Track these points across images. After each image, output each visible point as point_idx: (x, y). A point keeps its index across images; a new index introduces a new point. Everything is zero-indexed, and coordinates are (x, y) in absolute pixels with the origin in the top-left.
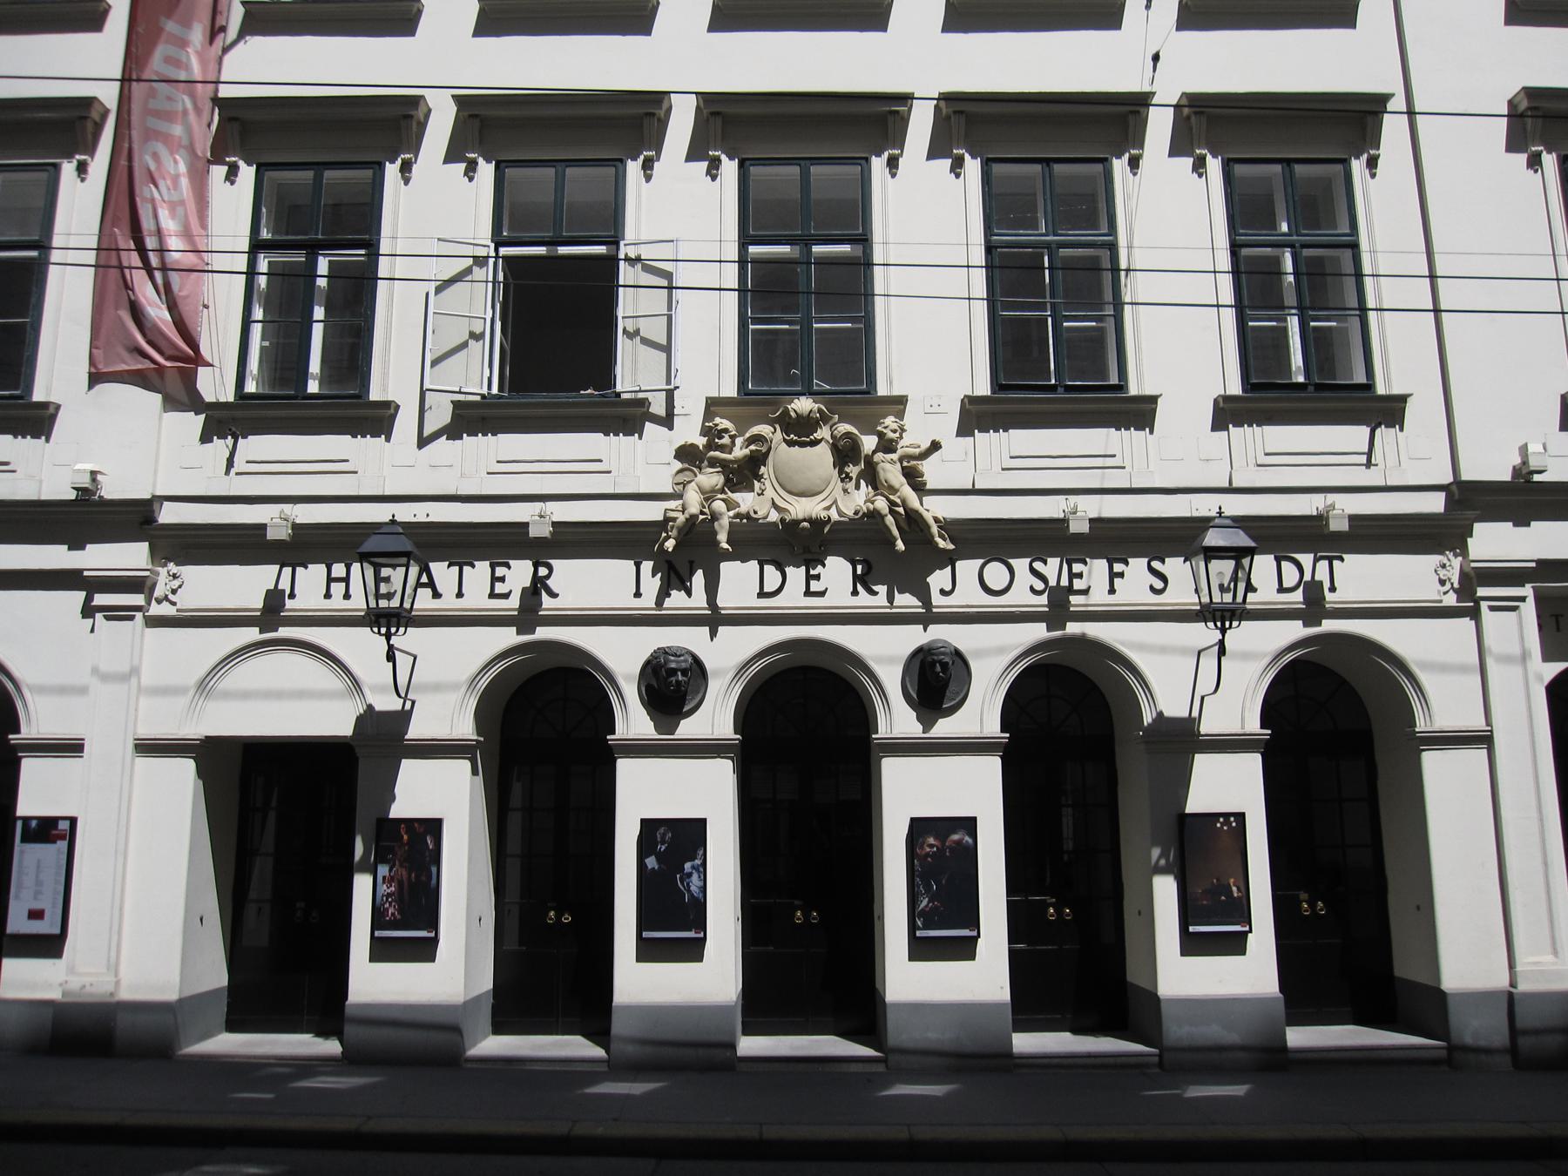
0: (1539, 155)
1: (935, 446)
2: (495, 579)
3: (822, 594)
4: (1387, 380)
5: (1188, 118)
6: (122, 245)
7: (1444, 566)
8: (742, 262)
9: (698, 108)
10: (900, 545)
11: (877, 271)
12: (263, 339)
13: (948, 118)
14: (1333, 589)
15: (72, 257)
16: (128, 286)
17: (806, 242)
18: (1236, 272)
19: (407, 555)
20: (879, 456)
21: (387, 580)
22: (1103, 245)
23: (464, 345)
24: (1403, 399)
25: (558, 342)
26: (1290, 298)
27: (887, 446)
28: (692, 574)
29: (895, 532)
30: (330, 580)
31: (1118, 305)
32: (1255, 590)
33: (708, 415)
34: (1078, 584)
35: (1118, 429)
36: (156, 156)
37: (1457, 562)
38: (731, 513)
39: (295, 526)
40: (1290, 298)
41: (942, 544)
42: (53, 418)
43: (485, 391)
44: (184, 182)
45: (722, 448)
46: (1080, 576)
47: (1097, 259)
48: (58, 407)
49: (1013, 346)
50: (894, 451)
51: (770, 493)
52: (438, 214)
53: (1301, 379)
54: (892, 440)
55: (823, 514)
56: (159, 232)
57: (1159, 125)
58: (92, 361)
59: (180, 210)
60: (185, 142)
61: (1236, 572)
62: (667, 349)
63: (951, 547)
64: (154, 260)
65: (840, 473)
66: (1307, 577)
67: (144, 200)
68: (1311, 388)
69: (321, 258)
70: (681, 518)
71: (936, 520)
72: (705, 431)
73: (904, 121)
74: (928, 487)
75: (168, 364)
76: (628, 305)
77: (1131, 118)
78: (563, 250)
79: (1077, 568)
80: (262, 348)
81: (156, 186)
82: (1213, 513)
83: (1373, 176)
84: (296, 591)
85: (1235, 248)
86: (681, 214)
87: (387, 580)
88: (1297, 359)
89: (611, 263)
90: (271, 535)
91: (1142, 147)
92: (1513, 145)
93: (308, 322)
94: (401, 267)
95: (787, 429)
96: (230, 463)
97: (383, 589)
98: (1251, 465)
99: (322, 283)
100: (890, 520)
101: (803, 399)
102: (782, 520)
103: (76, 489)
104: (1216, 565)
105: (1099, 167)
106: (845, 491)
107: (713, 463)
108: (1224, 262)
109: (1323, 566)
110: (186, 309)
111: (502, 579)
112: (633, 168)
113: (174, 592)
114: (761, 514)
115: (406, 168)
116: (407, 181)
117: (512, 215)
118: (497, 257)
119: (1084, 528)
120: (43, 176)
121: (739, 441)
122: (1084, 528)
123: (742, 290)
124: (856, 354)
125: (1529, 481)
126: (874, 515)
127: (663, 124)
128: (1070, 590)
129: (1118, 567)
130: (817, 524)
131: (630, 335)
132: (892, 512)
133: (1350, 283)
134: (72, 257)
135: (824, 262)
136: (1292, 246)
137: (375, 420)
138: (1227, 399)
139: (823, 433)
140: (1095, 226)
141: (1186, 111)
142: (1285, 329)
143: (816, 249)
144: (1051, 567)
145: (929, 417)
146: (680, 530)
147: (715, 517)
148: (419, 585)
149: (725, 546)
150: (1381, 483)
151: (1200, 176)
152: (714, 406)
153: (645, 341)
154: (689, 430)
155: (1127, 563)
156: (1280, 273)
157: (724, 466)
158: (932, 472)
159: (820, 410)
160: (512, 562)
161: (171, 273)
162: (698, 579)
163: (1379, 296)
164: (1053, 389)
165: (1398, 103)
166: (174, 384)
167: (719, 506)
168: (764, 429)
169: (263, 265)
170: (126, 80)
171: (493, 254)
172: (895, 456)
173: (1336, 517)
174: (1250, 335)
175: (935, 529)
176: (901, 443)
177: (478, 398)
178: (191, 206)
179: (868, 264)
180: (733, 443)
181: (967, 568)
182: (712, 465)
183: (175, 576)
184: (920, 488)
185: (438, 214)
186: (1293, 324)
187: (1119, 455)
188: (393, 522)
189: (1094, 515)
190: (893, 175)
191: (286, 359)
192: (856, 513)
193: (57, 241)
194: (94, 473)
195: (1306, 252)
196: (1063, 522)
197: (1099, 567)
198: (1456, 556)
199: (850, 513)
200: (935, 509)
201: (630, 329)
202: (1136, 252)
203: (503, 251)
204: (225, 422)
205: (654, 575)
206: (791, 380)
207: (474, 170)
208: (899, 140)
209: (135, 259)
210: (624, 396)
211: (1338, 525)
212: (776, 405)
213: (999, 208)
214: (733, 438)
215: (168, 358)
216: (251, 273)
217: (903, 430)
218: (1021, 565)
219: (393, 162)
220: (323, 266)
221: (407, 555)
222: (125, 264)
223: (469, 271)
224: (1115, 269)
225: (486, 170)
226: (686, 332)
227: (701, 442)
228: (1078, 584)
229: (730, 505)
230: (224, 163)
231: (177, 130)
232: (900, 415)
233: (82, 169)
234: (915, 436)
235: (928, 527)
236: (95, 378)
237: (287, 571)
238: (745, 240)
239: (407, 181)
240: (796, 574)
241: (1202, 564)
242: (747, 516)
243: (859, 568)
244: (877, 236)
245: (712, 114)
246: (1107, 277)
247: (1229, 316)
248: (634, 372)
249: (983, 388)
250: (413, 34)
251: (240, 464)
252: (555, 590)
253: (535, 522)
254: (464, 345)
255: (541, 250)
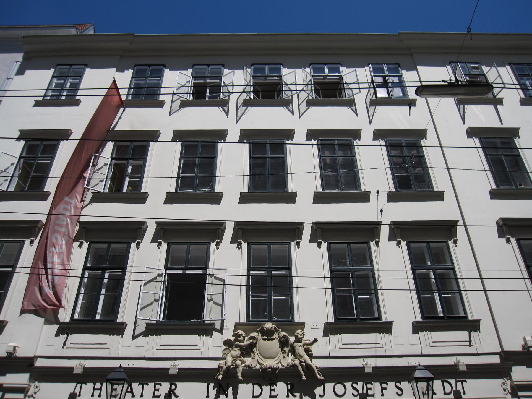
0: (509, 238)
1: (316, 340)
2: (155, 390)
3: (276, 397)
4: (472, 315)
5: (394, 229)
6: (41, 267)
7: (504, 384)
8: (248, 275)
9: (234, 226)
10: (304, 378)
11: (294, 279)
12: (83, 300)
13: (316, 230)
14: (464, 393)
15: (23, 270)
16: (40, 280)
17: (270, 270)
18: (415, 278)
19: (124, 380)
20: (296, 344)
21: (116, 390)
22: (369, 270)
23: (152, 303)
24: (478, 321)
25: (184, 304)
26: (434, 287)
27: (298, 340)
28: (228, 388)
29: (302, 372)
30: (94, 389)
31: (376, 290)
32: (435, 394)
33: (236, 329)
34: (370, 392)
35: (380, 334)
36: (56, 238)
37: (508, 382)
38: (243, 365)
39: (85, 368)
40: (434, 287)
41: (319, 377)
42: (5, 326)
43: (158, 319)
44: (64, 246)
45: (240, 341)
46: (370, 389)
47: (368, 275)
48: (7, 322)
49: (341, 305)
50: (301, 342)
51: (257, 358)
52: (147, 259)
53: (442, 315)
54: (300, 338)
55: (276, 366)
56: (53, 263)
57: (384, 231)
58: (23, 306)
59: (62, 256)
60: (67, 233)
61: (427, 387)
62: (222, 306)
63: (323, 378)
64: (49, 271)
65: (282, 350)
66: (454, 389)
67: (50, 252)
68: (446, 318)
69: (106, 273)
70: (225, 367)
71: (317, 368)
72: (234, 335)
73: (301, 231)
74: (314, 355)
75: (49, 307)
76: (208, 290)
77: (375, 229)
78: (188, 272)
79: (369, 386)
80: (82, 303)
81: (55, 248)
82: (417, 364)
83: (456, 246)
84: (81, 394)
85: (413, 270)
86: (228, 261)
87: (116, 390)
88: (439, 308)
89: (204, 276)
90: (75, 371)
91: (379, 238)
92: (501, 235)
93: (99, 294)
94: (133, 276)
95: (263, 335)
96: (65, 344)
97: (114, 393)
98: (428, 347)
99: (106, 281)
100: (300, 368)
101: (269, 323)
102: (261, 368)
103: (8, 353)
104: (420, 384)
105: (366, 245)
106: (284, 357)
107: (237, 346)
108: (410, 275)
109: (459, 384)
110: (58, 289)
111: (158, 390)
112: (213, 245)
113: (35, 393)
114: (254, 365)
115: (138, 244)
116: (138, 248)
117: (171, 261)
118: (166, 273)
119: (371, 371)
120: (19, 244)
121: (246, 338)
122: (371, 371)
123: (248, 286)
124: (286, 309)
125: (529, 351)
126: (294, 366)
127: (223, 231)
128: (367, 395)
129: (384, 386)
130: (274, 369)
131: (209, 301)
132: (301, 365)
133: (454, 281)
134: (23, 270)
135: (276, 276)
136: (433, 269)
137: (118, 329)
138: (417, 322)
139: (276, 336)
140: (366, 264)
141: (393, 226)
142: (434, 297)
143: (273, 272)
144: (360, 386)
145: (313, 331)
146: (224, 371)
147: (237, 366)
148: (127, 392)
149: (240, 378)
150: (475, 352)
151: (399, 247)
152: (237, 326)
153: (214, 303)
154: (228, 335)
155: (387, 384)
156: (430, 278)
157: (241, 347)
158: (315, 350)
159: (275, 327)
160: (162, 383)
161: (55, 277)
162: (230, 391)
163: (464, 286)
164: (356, 319)
165: (461, 223)
166: (50, 314)
167: (238, 362)
168: (255, 334)
169: (86, 275)
170: (50, 214)
171: (164, 272)
172: (301, 344)
173: (462, 365)
174: (422, 300)
175: (316, 371)
176: (304, 339)
177: (155, 322)
178: (65, 254)
179: (290, 276)
180: (244, 339)
181: (329, 386)
182: (236, 347)
183: (37, 387)
184: (311, 356)
185: (147, 259)
186: (436, 295)
187: (381, 343)
188: (120, 367)
189: (374, 365)
190: (298, 248)
191: (90, 307)
192: (288, 365)
193: (19, 265)
194: (15, 347)
195: (438, 271)
196: (362, 369)
197: (377, 385)
198: (508, 379)
199: (286, 365)
200: (317, 364)
201: (209, 299)
202: (381, 272)
203: (168, 272)
204: (65, 329)
205: (214, 389)
206: (265, 317)
207: (160, 245)
208: (300, 237)
209: (43, 271)
210: (206, 322)
211: (463, 368)
212: (259, 325)
213: (334, 258)
214: (244, 337)
215: (49, 305)
216: (82, 277)
217: (304, 335)
218: (348, 385)
219: (134, 242)
220: (107, 275)
221: (124, 380)
222: (40, 273)
223: (156, 278)
224: (374, 278)
225: (164, 245)
226: (229, 301)
227: (233, 339)
228: (370, 392)
229: (243, 362)
230: (78, 242)
231: (63, 230)
232: (303, 329)
233: (32, 242)
234: (308, 337)
235: (314, 371)
236: (23, 312)
237: (79, 385)
238: (249, 269)
239: (138, 248)
240: (266, 389)
241: (415, 384)
242: (249, 366)
243: (289, 386)
244: (293, 268)
245: (239, 228)
246: (371, 280)
247: (414, 293)
248: (210, 314)
249: (331, 320)
250: (144, 203)
251: (68, 345)
252: (177, 394)
253: (172, 368)
254: (152, 303)
255: (181, 272)
